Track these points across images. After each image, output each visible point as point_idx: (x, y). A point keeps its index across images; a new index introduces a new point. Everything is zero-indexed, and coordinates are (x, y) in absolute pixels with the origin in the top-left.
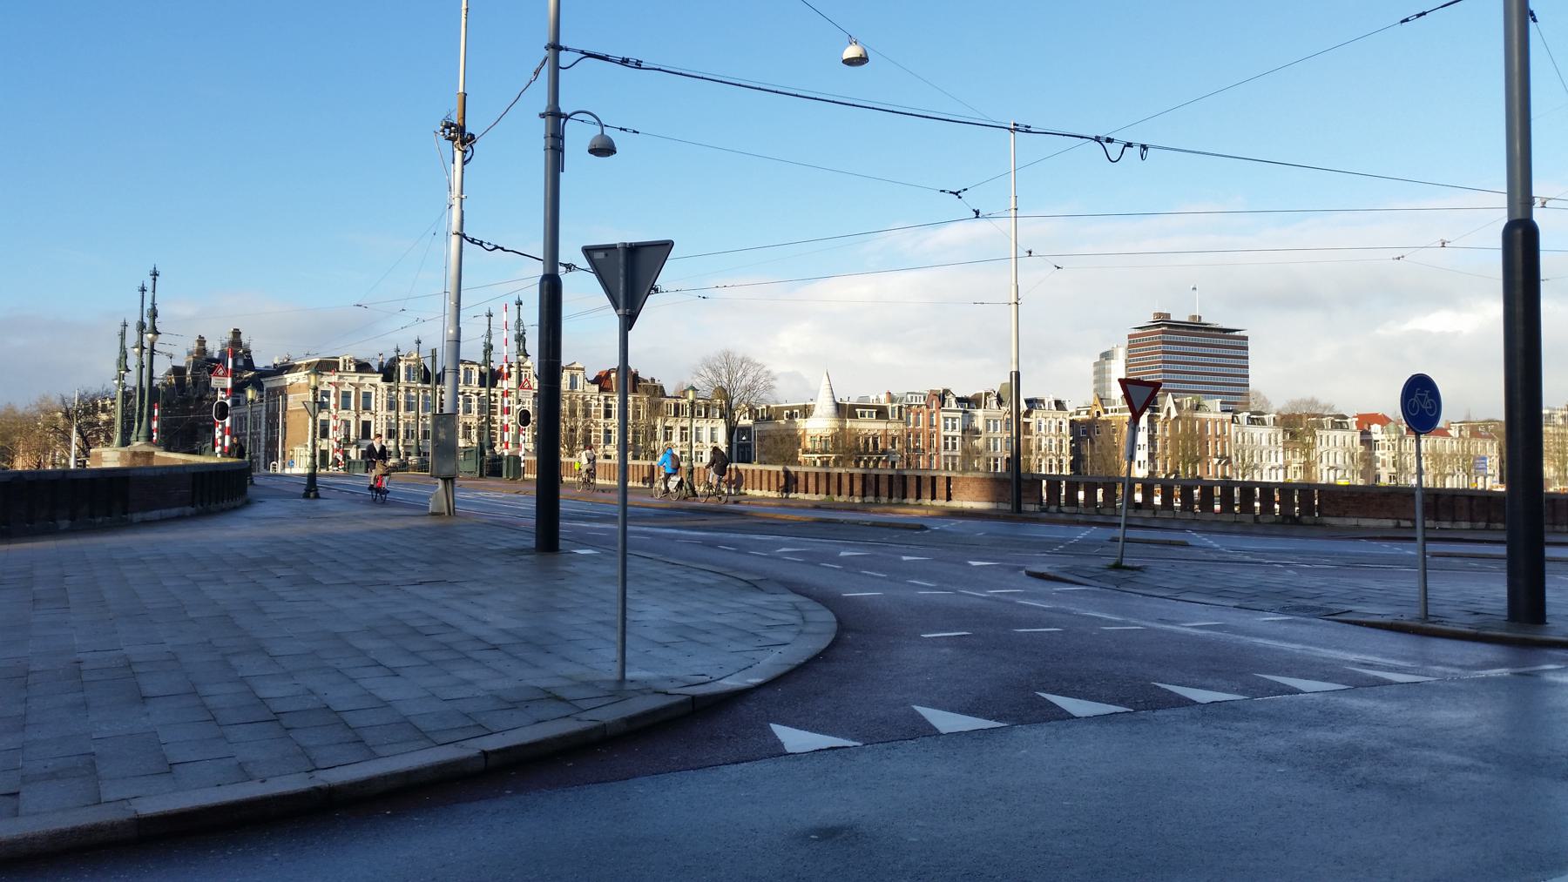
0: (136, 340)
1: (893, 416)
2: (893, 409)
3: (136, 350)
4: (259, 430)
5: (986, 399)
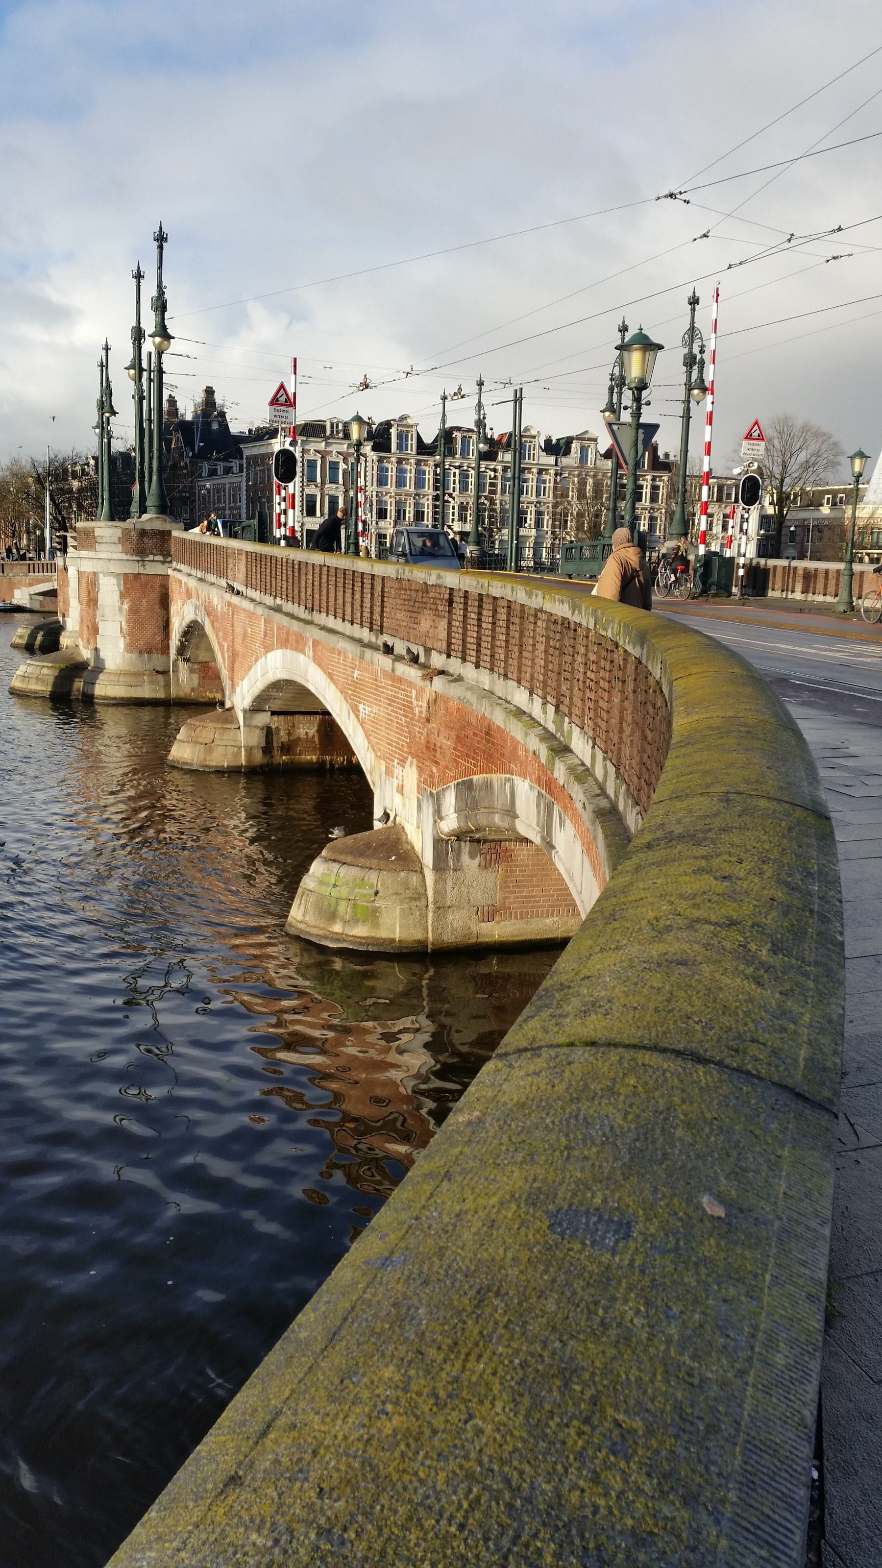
0: (132, 356)
3: (97, 430)
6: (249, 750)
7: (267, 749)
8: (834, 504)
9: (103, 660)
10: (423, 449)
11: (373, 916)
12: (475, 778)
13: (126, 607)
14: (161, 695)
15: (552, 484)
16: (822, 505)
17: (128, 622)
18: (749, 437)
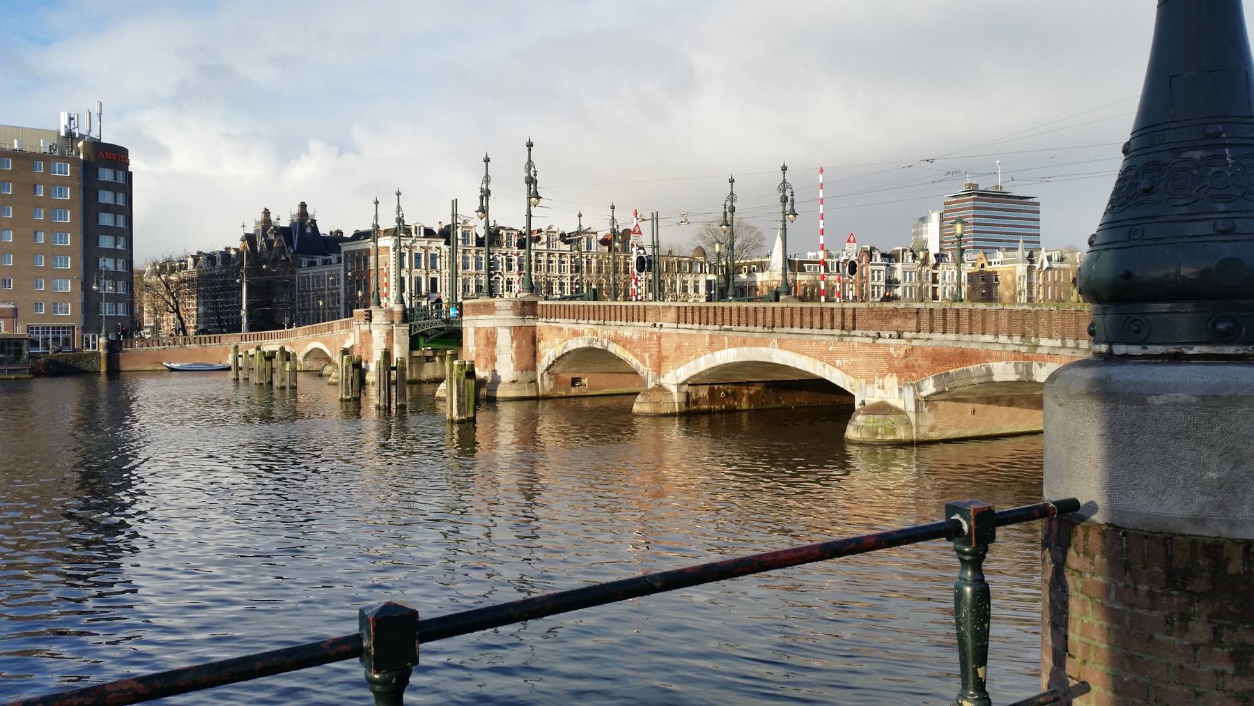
1: (833, 269)
2: (833, 263)
4: (337, 286)
5: (903, 254)
6: (680, 404)
7: (687, 404)
8: (749, 272)
9: (500, 377)
10: (480, 242)
11: (893, 432)
12: (950, 371)
13: (514, 345)
14: (534, 394)
15: (569, 264)
16: (741, 273)
17: (516, 354)
18: (849, 241)
